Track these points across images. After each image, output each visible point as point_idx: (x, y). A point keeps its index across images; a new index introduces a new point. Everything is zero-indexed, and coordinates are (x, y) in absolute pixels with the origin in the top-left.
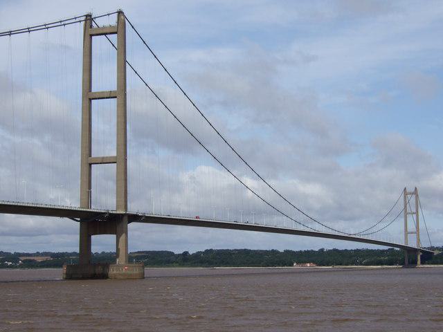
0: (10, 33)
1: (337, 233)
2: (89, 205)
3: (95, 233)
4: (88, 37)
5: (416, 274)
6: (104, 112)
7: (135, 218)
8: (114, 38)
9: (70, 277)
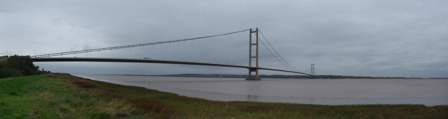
0: (236, 33)
3: (255, 75)
4: (250, 46)
5: (99, 50)
6: (254, 47)
7: (259, 68)
8: (256, 33)
9: (246, 80)
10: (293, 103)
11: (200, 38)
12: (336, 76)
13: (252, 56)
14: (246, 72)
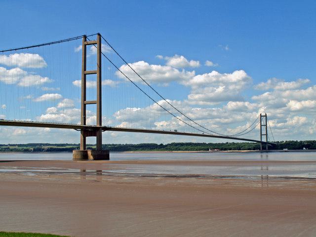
7: (106, 129)
10: (145, 159)
11: (43, 45)
14: (74, 138)
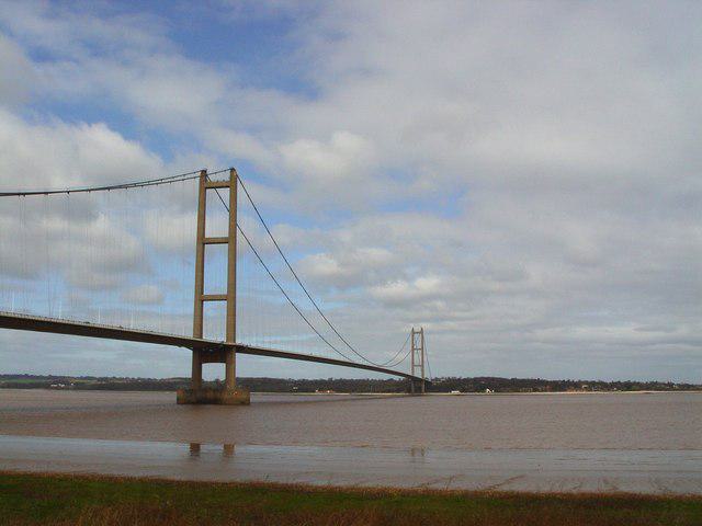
1: (365, 363)
2: (201, 337)
5: (306, 402)
9: (179, 401)
12: (514, 381)
13: (207, 236)
14: (178, 363)
